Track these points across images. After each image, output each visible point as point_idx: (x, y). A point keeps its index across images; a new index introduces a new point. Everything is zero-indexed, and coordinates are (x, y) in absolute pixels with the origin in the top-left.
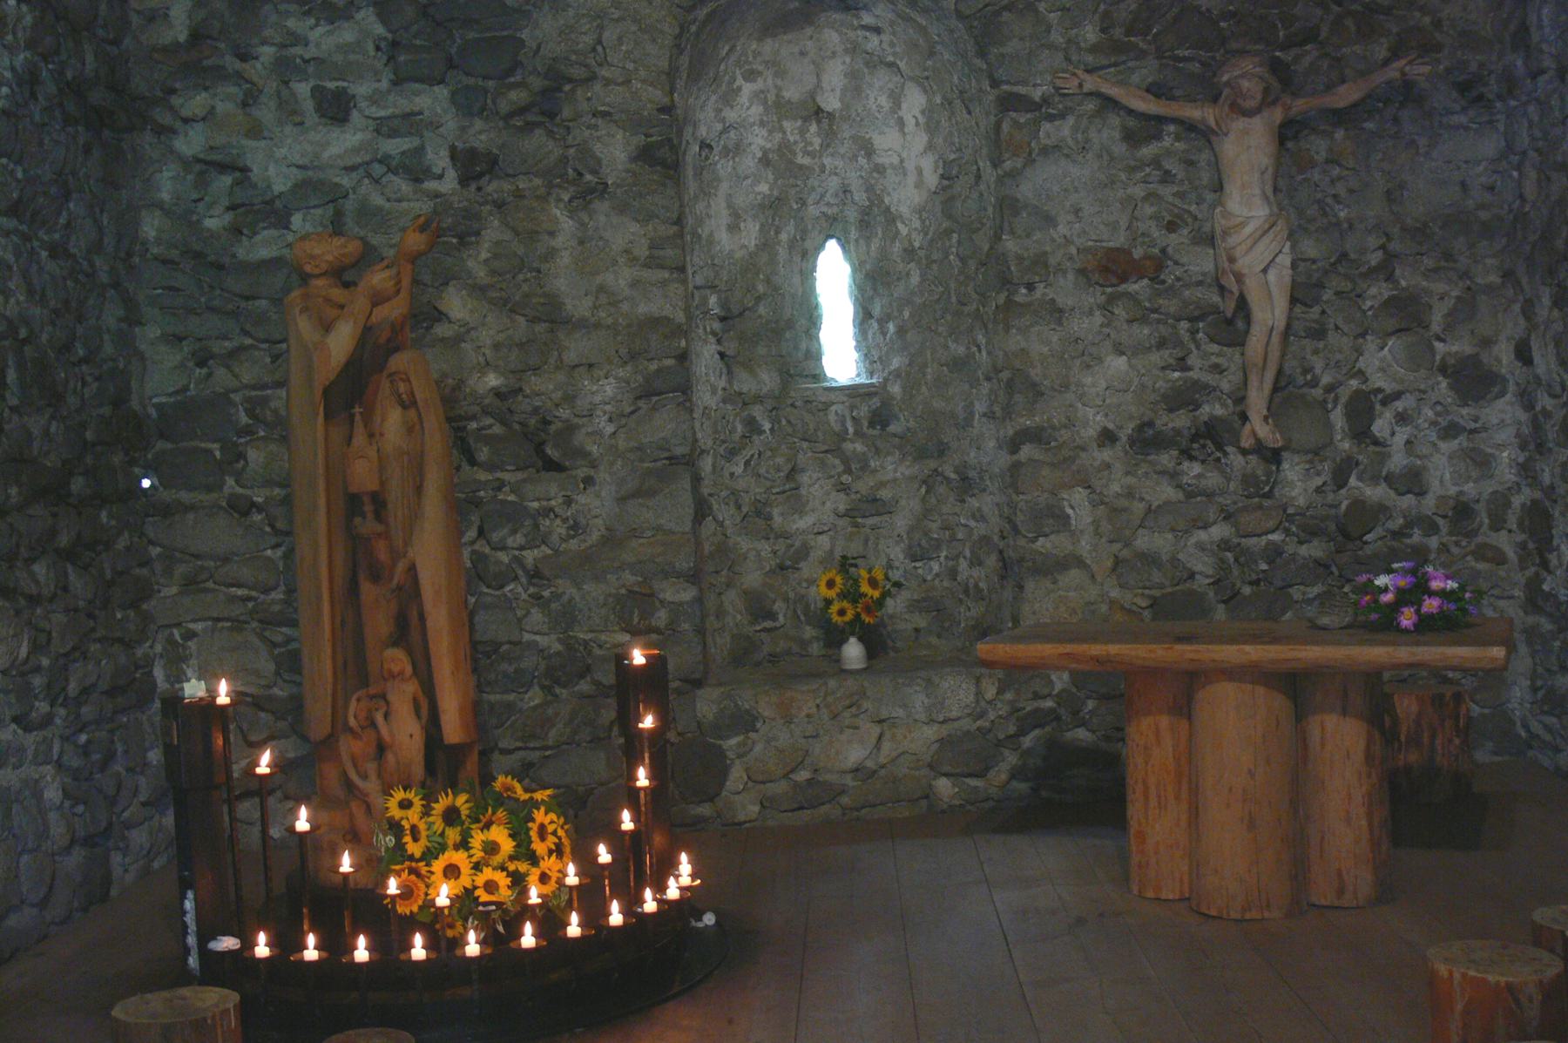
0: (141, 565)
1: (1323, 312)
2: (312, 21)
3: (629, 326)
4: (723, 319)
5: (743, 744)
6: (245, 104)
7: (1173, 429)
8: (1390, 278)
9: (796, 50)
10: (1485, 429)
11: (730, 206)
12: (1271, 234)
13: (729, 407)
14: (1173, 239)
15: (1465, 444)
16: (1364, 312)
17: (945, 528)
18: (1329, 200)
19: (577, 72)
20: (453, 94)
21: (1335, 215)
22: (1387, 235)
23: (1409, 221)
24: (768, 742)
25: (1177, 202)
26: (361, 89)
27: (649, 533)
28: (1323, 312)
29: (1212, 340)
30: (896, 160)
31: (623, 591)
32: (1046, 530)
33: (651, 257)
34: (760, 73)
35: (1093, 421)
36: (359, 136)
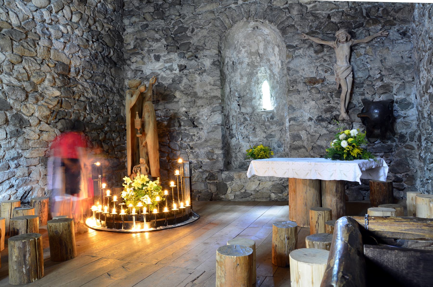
0: (123, 144)
1: (364, 90)
2: (154, 42)
3: (210, 98)
4: (239, 97)
5: (231, 183)
6: (142, 59)
7: (326, 117)
8: (382, 80)
9: (253, 41)
10: (409, 116)
11: (240, 74)
12: (347, 70)
13: (240, 115)
14: (326, 74)
15: (402, 120)
16: (375, 89)
17: (284, 140)
18: (366, 63)
19: (201, 48)
20: (178, 54)
21: (367, 67)
22: (381, 71)
23: (387, 67)
24: (236, 183)
25: (328, 66)
26: (162, 54)
27: (213, 139)
28: (364, 90)
29: (336, 97)
30: (274, 63)
31: (208, 151)
32: (296, 140)
33: (214, 84)
34: (246, 47)
35: (307, 116)
36: (161, 63)
